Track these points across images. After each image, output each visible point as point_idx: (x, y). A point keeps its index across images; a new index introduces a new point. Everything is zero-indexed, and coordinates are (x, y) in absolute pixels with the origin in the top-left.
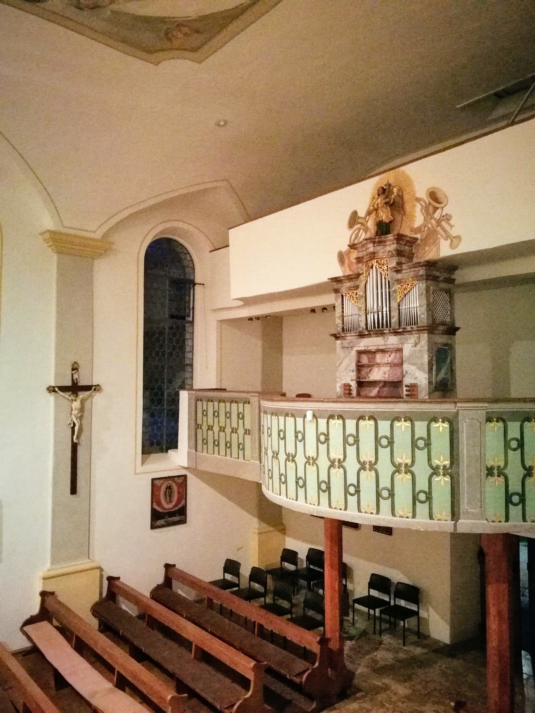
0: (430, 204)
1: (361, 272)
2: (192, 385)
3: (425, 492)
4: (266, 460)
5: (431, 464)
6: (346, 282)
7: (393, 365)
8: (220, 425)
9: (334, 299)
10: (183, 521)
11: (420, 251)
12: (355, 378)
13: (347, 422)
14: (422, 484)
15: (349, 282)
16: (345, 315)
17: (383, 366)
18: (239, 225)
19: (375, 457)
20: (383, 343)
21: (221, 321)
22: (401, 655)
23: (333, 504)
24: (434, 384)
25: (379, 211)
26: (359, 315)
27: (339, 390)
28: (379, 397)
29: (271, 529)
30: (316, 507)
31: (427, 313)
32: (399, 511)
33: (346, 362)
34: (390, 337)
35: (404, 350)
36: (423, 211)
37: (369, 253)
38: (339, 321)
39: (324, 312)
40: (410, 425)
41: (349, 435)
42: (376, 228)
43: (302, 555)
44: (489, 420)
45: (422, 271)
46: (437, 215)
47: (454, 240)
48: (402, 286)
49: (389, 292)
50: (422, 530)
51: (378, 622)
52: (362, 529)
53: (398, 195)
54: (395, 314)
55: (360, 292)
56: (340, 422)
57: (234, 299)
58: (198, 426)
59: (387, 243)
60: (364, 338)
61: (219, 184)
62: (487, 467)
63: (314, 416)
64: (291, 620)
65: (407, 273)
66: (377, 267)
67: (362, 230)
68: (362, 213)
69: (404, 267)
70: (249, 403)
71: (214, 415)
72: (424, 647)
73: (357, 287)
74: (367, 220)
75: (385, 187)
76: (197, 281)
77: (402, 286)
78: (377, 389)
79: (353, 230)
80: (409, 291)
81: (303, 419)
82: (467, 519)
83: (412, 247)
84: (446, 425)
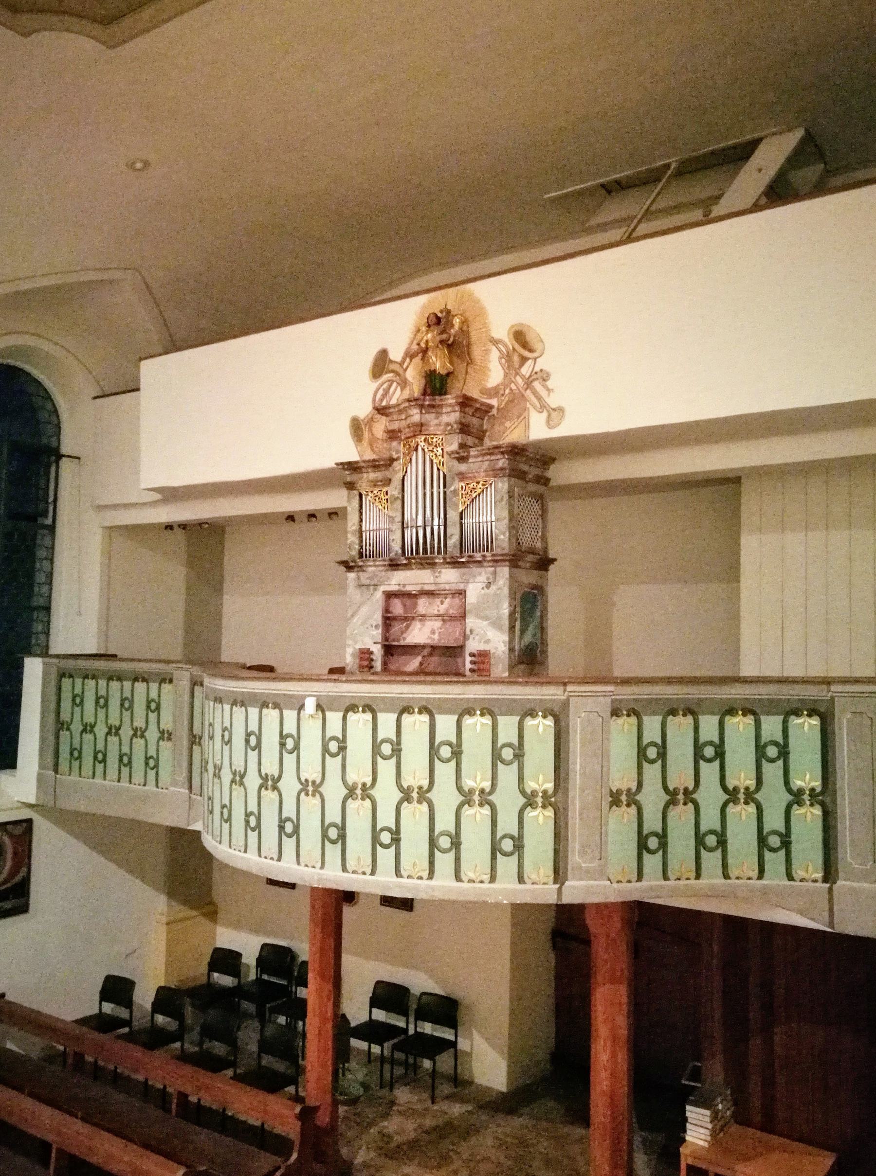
0: (514, 349)
1: (395, 456)
2: (47, 647)
3: (512, 837)
4: (217, 788)
5: (523, 788)
6: (368, 472)
7: (446, 618)
8: (135, 724)
9: (345, 498)
10: (23, 909)
11: (497, 427)
12: (379, 639)
13: (381, 716)
14: (508, 824)
15: (374, 472)
16: (364, 529)
17: (431, 620)
18: (152, 357)
19: (428, 779)
20: (432, 580)
21: (111, 529)
22: (429, 1122)
23: (351, 864)
24: (516, 654)
25: (430, 353)
26: (390, 530)
27: (349, 660)
28: (421, 671)
29: (194, 913)
30: (317, 870)
31: (510, 533)
32: (467, 872)
33: (364, 610)
34: (443, 570)
35: (468, 593)
36: (503, 361)
37: (412, 424)
38: (352, 539)
39: (311, 521)
40: (490, 722)
41: (383, 741)
42: (423, 381)
43: (250, 958)
44: (615, 713)
45: (502, 462)
46: (526, 370)
47: (554, 415)
48: (468, 484)
49: (445, 493)
50: (505, 902)
51: (387, 1067)
52: (362, 901)
53: (461, 329)
54: (454, 531)
55: (393, 490)
56: (368, 716)
57: (145, 489)
58: (62, 724)
59: (444, 410)
60: (398, 570)
61: (118, 275)
62: (611, 791)
63: (319, 707)
64: (236, 1078)
65: (477, 464)
66: (426, 450)
67: (395, 384)
68: (396, 355)
69: (473, 452)
70: (171, 681)
71: (122, 705)
72: (463, 1101)
73: (388, 482)
74: (405, 367)
75: (440, 315)
76: (65, 449)
77: (468, 484)
78: (419, 659)
79: (378, 383)
80: (479, 495)
81: (296, 712)
82: (581, 879)
83: (483, 419)
84: (550, 722)
